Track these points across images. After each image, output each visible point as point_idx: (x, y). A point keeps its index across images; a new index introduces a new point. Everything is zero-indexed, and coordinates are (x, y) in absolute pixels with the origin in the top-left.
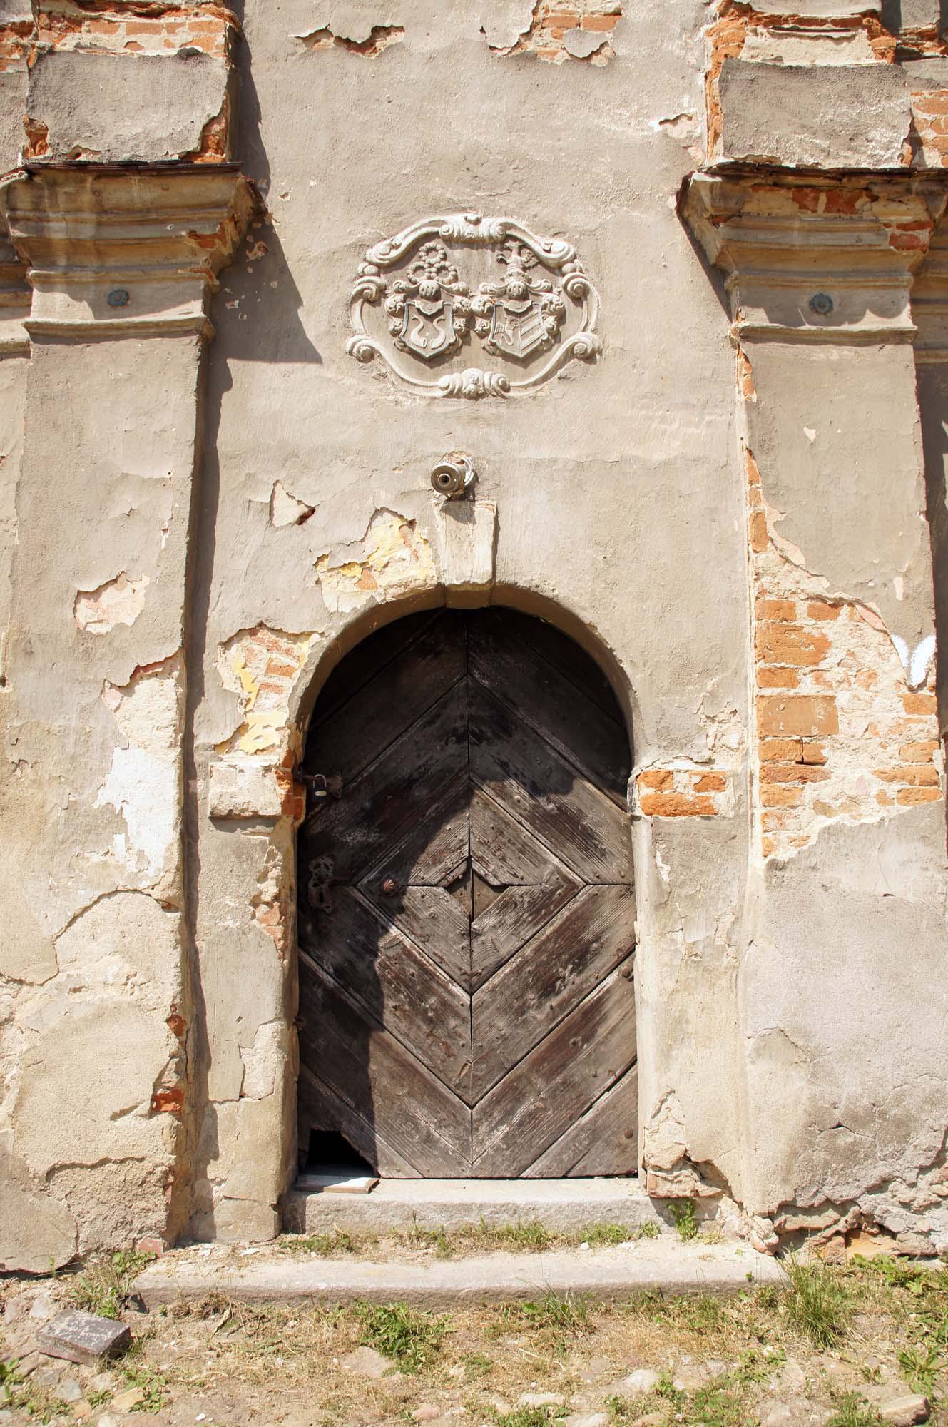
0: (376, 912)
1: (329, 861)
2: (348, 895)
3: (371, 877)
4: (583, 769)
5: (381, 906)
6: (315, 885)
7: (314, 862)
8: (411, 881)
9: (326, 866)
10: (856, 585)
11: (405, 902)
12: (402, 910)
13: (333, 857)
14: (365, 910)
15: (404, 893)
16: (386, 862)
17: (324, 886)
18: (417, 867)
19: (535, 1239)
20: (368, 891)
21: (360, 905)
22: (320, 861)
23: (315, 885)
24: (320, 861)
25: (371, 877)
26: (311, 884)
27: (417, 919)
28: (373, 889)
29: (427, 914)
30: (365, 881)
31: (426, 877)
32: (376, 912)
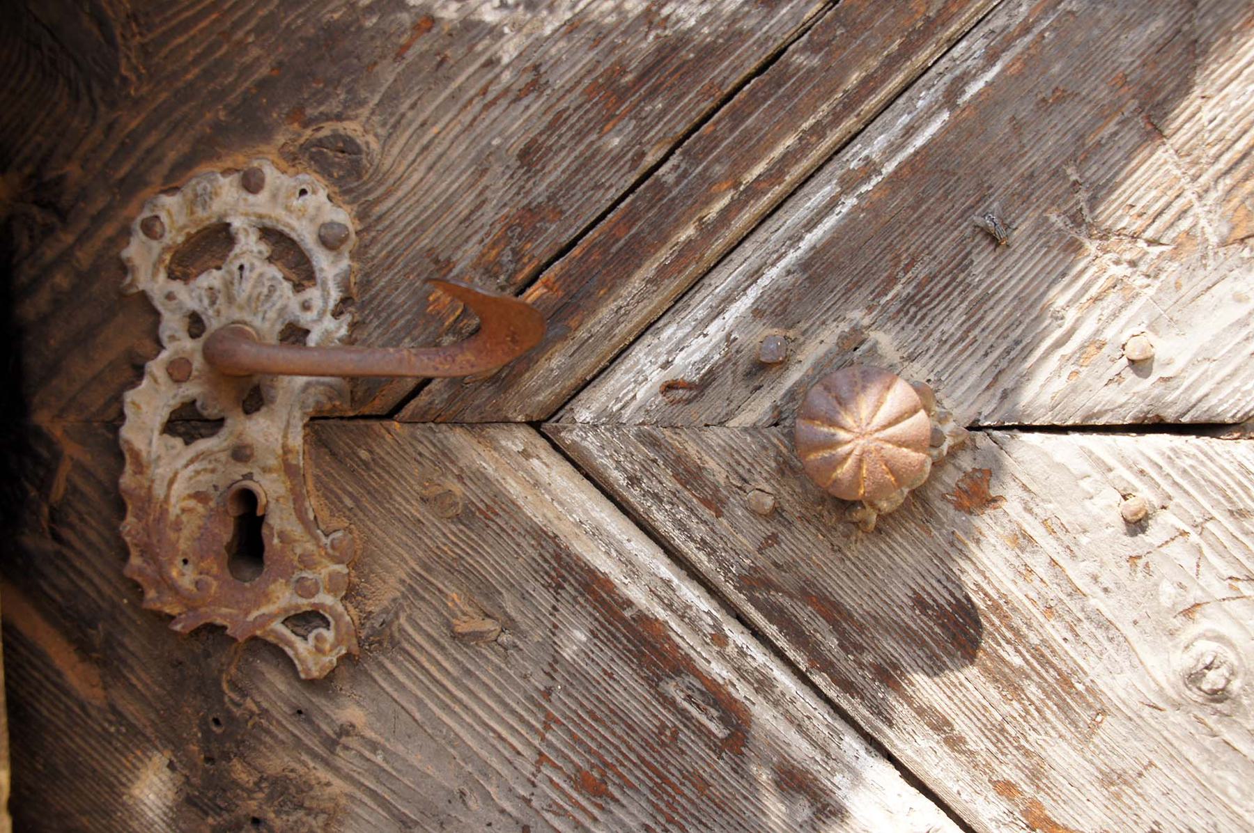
0: (731, 657)
1: (309, 207)
2: (485, 513)
3: (689, 344)
4: (919, 141)
5: (775, 602)
6: (187, 423)
7: (173, 212)
8: (1043, 390)
9: (280, 243)
10: (247, 498)
11: (991, 566)
12: (958, 630)
13: (342, 165)
14: (647, 647)
15: (978, 494)
16: (821, 215)
17: (274, 431)
18: (1099, 265)
19: (1021, 279)
20: (660, 479)
21: (594, 590)
22: (226, 197)
23: (187, 423)
24: (226, 197)
25: (689, 344)
26: (148, 407)
27: (1068, 694)
28: (710, 451)
29: (1164, 665)
30: (639, 381)
31: (1171, 351)
32: (731, 657)
